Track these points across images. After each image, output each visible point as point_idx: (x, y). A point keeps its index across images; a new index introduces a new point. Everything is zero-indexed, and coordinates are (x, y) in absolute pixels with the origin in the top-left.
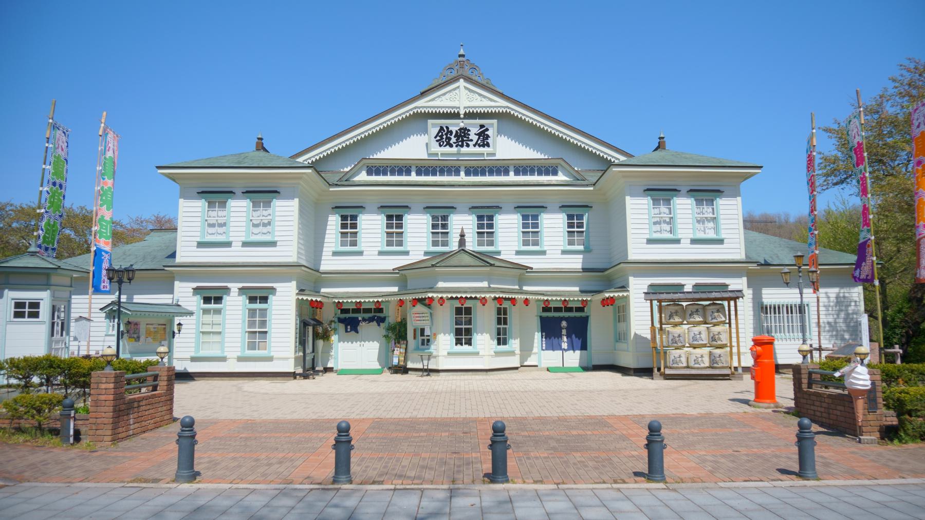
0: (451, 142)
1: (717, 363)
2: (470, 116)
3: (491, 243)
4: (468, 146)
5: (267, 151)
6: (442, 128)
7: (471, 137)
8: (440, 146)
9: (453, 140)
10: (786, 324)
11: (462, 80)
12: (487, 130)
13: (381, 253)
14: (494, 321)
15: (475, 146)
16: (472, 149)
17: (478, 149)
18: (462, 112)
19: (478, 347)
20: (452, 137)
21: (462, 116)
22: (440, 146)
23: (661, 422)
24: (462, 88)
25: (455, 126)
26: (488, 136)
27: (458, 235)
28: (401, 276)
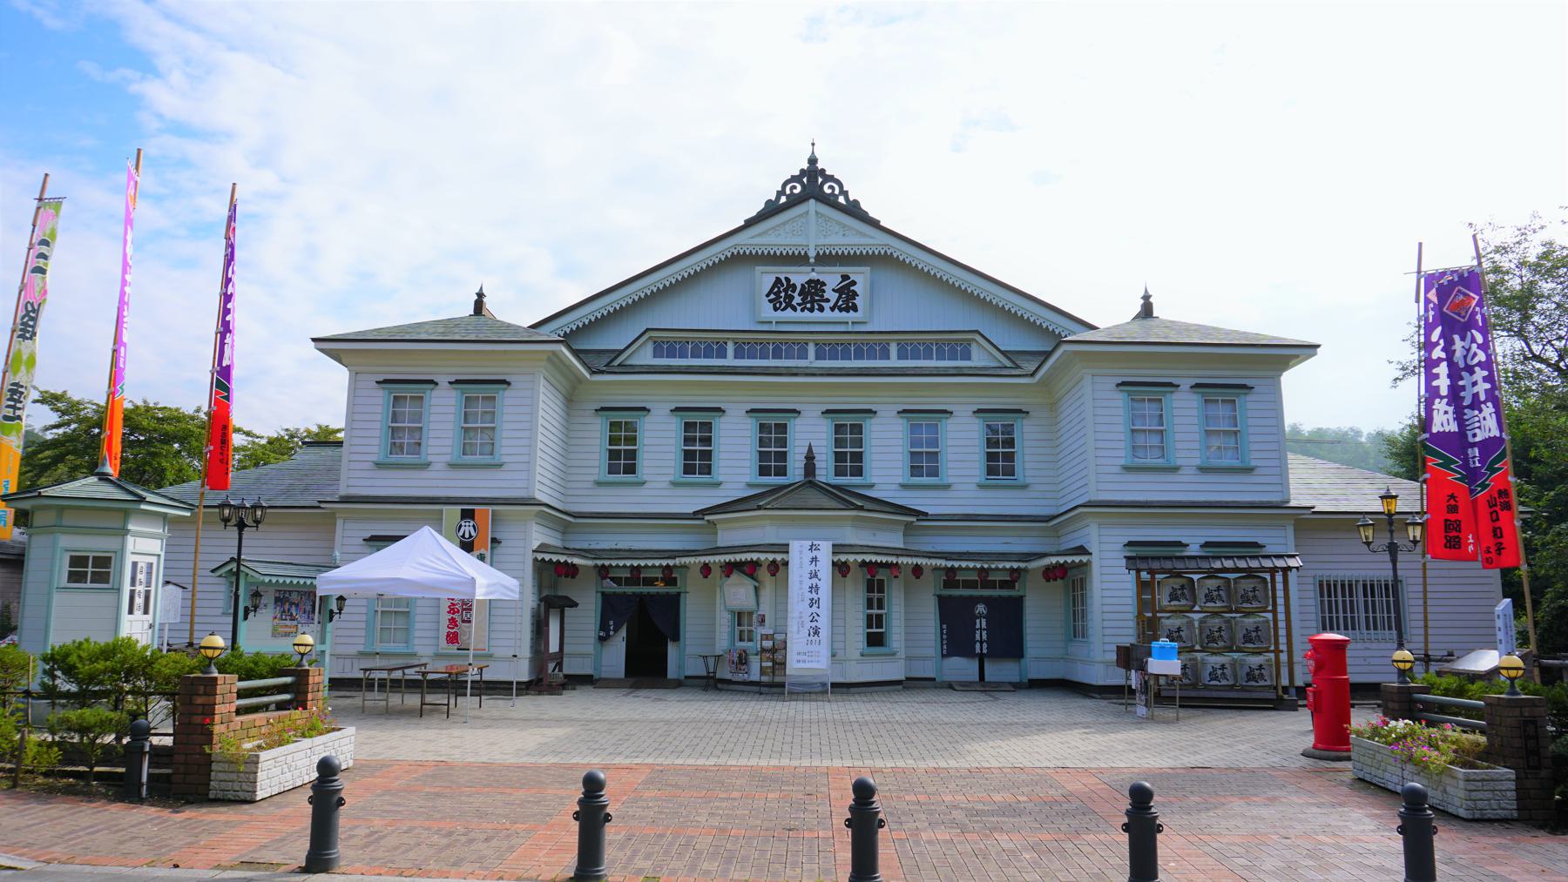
2: (825, 259)
4: (821, 309)
5: (480, 295)
7: (826, 296)
8: (776, 309)
9: (797, 299)
10: (1341, 615)
11: (812, 201)
12: (854, 283)
15: (832, 309)
16: (828, 314)
17: (837, 314)
18: (812, 254)
22: (776, 309)
24: (812, 212)
25: (799, 277)
26: (855, 294)
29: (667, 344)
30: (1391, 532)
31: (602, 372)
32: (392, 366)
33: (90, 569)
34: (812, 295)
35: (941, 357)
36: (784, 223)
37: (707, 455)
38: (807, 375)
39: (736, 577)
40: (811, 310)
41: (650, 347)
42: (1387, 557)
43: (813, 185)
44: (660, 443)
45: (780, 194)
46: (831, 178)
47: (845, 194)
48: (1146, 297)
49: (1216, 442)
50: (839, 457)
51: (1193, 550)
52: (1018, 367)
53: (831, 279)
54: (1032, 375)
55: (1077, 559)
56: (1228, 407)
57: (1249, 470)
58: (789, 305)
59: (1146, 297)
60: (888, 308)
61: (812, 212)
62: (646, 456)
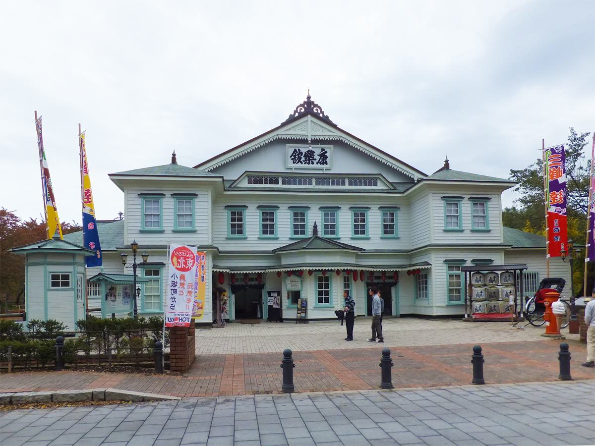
0: (302, 160)
1: (492, 311)
2: (315, 142)
3: (333, 233)
4: (313, 163)
5: (174, 155)
6: (295, 150)
7: (315, 158)
8: (294, 163)
9: (303, 159)
10: (530, 286)
11: (309, 116)
12: (326, 152)
13: (228, 239)
14: (343, 286)
16: (315, 166)
17: (319, 166)
18: (309, 139)
19: (334, 303)
20: (302, 157)
21: (310, 142)
22: (294, 163)
23: (481, 346)
24: (309, 121)
25: (304, 149)
26: (327, 157)
27: (312, 227)
28: (276, 254)
29: (255, 178)
30: (135, 256)
31: (229, 190)
32: (142, 186)
33: (60, 280)
34: (309, 157)
35: (365, 185)
36: (298, 125)
37: (272, 226)
38: (321, 192)
39: (293, 277)
40: (309, 164)
41: (246, 180)
42: (132, 269)
43: (309, 109)
44: (252, 219)
45: (295, 112)
46: (316, 106)
47: (322, 113)
48: (447, 161)
49: (476, 220)
50: (326, 226)
51: (469, 264)
52: (396, 189)
53: (317, 150)
54: (403, 193)
55: (426, 267)
56: (455, 206)
57: (489, 231)
58: (299, 161)
59: (447, 161)
60: (341, 164)
61: (309, 121)
62: (247, 226)
